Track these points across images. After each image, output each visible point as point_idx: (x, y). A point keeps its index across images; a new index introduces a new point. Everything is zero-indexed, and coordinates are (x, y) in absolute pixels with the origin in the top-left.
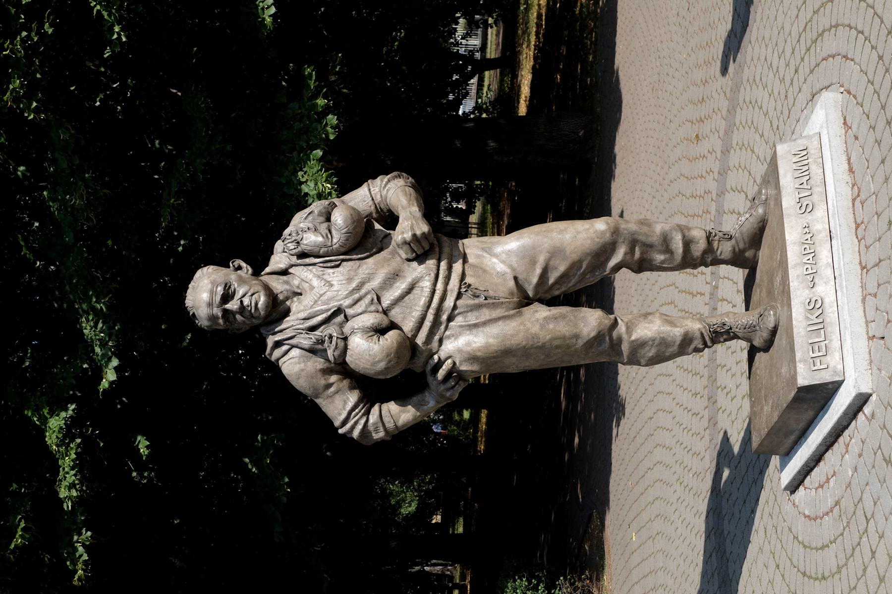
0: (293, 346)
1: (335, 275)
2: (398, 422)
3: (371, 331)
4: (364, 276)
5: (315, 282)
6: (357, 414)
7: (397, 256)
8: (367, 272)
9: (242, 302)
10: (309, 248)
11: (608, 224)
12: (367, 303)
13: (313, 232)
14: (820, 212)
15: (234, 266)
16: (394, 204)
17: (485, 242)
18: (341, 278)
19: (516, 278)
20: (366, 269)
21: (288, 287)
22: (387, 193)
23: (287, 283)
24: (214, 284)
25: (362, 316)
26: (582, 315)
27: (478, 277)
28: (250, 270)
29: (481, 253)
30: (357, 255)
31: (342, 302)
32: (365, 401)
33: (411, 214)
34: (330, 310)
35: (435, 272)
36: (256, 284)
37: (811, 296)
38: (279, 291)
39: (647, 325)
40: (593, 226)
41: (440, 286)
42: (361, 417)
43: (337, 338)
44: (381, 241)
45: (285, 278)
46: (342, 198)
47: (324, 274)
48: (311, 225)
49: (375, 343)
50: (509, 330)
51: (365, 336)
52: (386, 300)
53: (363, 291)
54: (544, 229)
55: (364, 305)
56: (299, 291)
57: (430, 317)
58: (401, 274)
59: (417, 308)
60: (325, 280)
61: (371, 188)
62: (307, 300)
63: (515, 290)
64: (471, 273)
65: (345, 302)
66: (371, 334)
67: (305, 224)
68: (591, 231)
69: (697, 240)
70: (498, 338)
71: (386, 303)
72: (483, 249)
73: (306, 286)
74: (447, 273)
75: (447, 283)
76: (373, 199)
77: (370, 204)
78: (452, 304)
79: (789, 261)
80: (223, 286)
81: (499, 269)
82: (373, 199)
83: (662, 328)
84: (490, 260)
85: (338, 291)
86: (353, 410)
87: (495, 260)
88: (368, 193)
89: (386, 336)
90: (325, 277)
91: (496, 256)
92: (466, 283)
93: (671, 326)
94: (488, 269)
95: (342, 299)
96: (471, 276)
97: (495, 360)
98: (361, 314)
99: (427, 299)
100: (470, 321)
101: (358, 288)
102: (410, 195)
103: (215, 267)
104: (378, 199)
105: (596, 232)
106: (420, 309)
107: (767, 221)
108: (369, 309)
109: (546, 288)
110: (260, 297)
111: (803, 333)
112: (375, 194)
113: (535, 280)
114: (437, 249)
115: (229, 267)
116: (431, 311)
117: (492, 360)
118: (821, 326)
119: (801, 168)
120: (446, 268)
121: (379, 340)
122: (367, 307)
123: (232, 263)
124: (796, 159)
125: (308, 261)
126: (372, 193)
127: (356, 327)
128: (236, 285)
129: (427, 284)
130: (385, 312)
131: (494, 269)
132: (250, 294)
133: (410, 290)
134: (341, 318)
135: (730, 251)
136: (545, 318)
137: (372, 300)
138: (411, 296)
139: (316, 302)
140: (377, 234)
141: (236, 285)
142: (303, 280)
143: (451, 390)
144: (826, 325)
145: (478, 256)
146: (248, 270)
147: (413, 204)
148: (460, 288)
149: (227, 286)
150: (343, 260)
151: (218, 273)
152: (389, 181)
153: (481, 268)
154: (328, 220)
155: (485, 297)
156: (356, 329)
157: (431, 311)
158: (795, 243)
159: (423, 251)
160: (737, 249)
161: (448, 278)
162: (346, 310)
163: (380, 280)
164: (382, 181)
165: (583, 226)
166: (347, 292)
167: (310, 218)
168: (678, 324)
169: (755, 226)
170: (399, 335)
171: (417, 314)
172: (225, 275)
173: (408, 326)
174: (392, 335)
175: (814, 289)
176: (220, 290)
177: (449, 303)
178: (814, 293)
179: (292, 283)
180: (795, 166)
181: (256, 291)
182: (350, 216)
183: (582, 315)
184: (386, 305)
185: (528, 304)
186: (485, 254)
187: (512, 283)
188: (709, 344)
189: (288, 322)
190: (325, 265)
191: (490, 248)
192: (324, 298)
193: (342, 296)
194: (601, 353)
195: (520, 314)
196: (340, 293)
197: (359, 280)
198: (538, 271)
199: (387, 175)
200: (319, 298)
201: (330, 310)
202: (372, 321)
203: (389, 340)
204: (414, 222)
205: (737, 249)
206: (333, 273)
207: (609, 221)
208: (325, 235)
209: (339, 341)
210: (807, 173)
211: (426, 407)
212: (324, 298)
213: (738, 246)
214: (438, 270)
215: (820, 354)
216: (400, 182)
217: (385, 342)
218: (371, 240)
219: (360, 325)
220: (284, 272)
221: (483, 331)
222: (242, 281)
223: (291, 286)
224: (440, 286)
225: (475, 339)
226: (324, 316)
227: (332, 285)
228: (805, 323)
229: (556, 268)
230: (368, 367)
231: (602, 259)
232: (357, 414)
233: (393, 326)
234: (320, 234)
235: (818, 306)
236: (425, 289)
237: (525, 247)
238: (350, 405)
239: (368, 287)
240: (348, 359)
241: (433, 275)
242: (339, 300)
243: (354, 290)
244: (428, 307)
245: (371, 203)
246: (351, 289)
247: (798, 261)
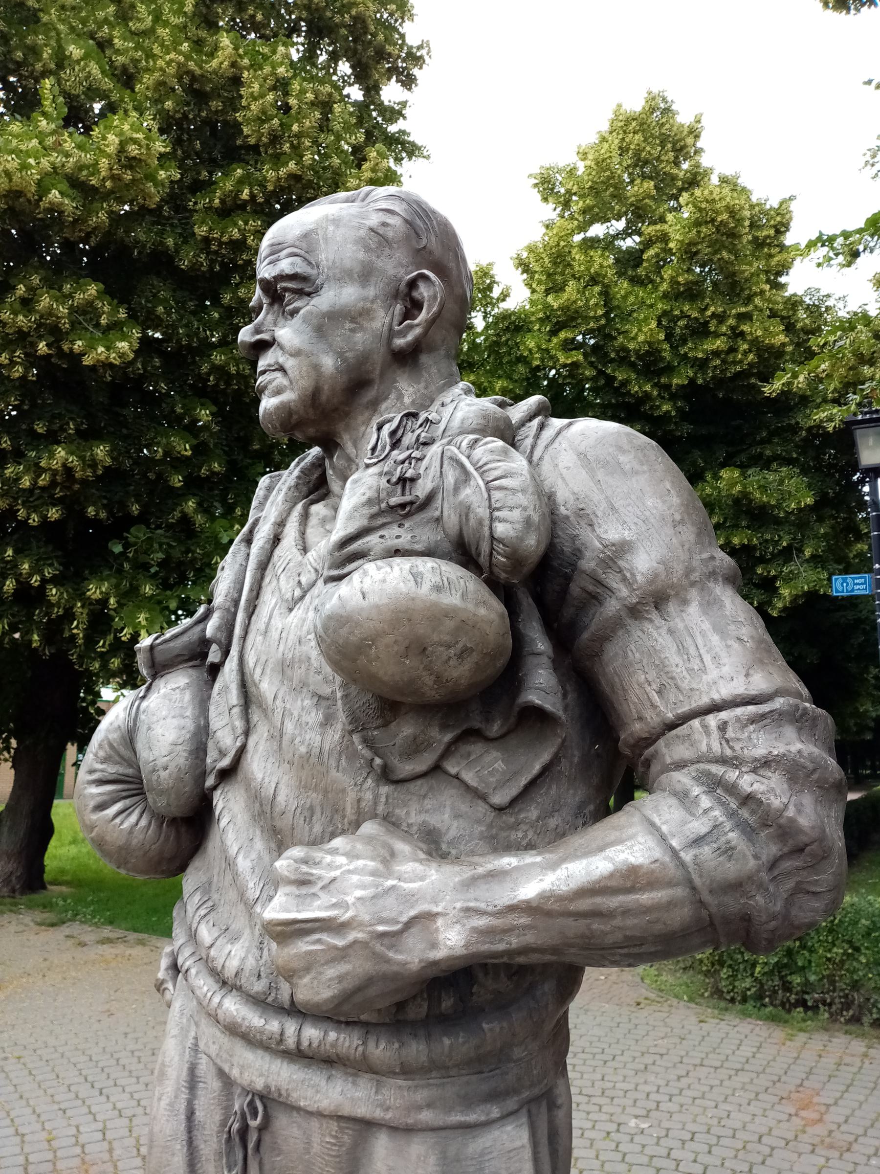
76: (672, 726)
77: (649, 714)
82: (672, 726)
88: (704, 700)
126: (696, 723)
245: (653, 719)
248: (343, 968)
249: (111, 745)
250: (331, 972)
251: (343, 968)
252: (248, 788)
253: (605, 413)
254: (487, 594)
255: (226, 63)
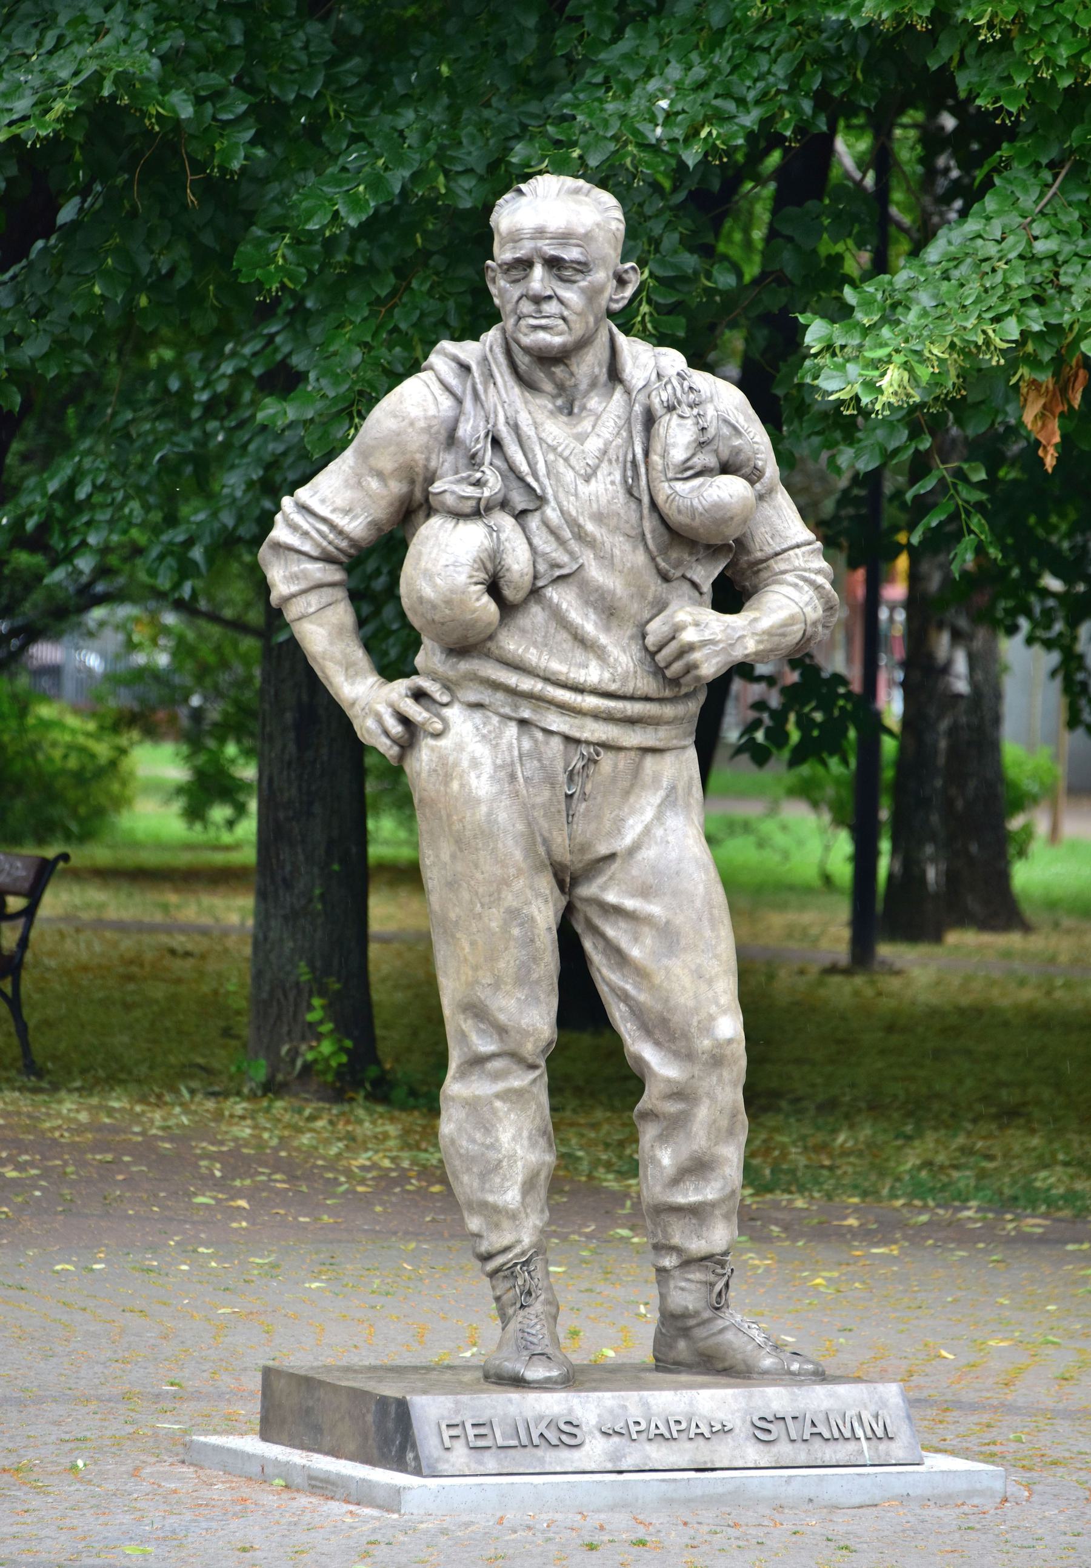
0: (459, 401)
1: (609, 486)
2: (311, 622)
3: (495, 567)
4: (608, 546)
5: (593, 445)
6: (324, 537)
7: (654, 611)
8: (617, 552)
9: (550, 298)
10: (662, 431)
11: (730, 1041)
12: (554, 555)
13: (695, 440)
14: (753, 1454)
15: (626, 271)
16: (764, 600)
17: (689, 793)
18: (603, 501)
19: (612, 856)
20: (622, 551)
21: (584, 386)
22: (791, 585)
23: (593, 385)
24: (586, 238)
25: (526, 546)
26: (542, 996)
27: (614, 780)
28: (616, 307)
29: (665, 784)
30: (653, 531)
31: (553, 503)
32: (352, 551)
33: (740, 638)
34: (537, 479)
35: (620, 693)
36: (587, 323)
37: (585, 1428)
38: (574, 368)
39: (525, 1134)
40: (725, 1012)
41: (591, 702)
42: (318, 545)
43: (480, 499)
44: (684, 576)
45: (604, 377)
46: (781, 488)
47: (610, 461)
48: (711, 432)
49: (471, 577)
50: (505, 846)
51: (484, 556)
52: (559, 594)
53: (574, 545)
54: (716, 912)
55: (548, 550)
56: (576, 410)
57: (527, 684)
58: (614, 623)
59: (545, 657)
60: (598, 467)
61: (804, 549)
62: (555, 430)
63: (590, 856)
64: (621, 765)
65: (554, 510)
66: (489, 566)
67: (715, 422)
68: (713, 1009)
69: (705, 1234)
70: (489, 822)
71: (553, 594)
72: (673, 789)
73: (586, 425)
74: (619, 716)
75: (596, 715)
76: (777, 554)
77: (766, 548)
78: (554, 728)
79: (656, 1393)
80: (582, 259)
81: (631, 822)
82: (777, 554)
83: (519, 1164)
84: (649, 804)
85: (576, 495)
86: (333, 527)
87: (649, 814)
88: (793, 542)
89: (486, 598)
90: (605, 465)
91: (659, 817)
92: (598, 754)
93: (524, 1184)
94: (632, 799)
95: (559, 504)
96: (615, 766)
97: (445, 818)
98: (530, 544)
99: (563, 678)
100: (522, 765)
101: (581, 535)
102: (784, 635)
103: (621, 234)
104: (778, 565)
105: (712, 1018)
106: (543, 663)
107: (749, 1378)
108: (540, 560)
109: (598, 922)
110: (561, 334)
111: (512, 1410)
112: (788, 559)
113: (611, 897)
114: (667, 693)
115: (623, 260)
116: (538, 686)
117: (443, 813)
118: (525, 1440)
119: (848, 1425)
120: (629, 713)
121: (476, 583)
122: (544, 554)
123: (633, 268)
124: (867, 1416)
125: (638, 427)
126: (791, 553)
127: (503, 536)
128: (583, 284)
129: (593, 674)
130: (535, 592)
131: (633, 812)
132: (566, 313)
133: (581, 640)
134: (520, 501)
135: (687, 1308)
136: (532, 919)
137: (559, 566)
138: (568, 645)
139: (554, 449)
140: (700, 568)
141: (583, 284)
142: (598, 417)
143: (379, 731)
144: (527, 1450)
145: (656, 779)
146: (617, 301)
147: (759, 642)
148: (588, 743)
149: (583, 267)
150: (639, 501)
151: (609, 242)
152: (818, 588)
153: (632, 786)
154: (726, 468)
155: (572, 795)
156: (498, 538)
157: (538, 686)
158: (691, 1404)
159: (662, 665)
160: (692, 1322)
161: (608, 718)
162: (537, 514)
163: (601, 579)
164: (819, 572)
165: (725, 992)
166: (574, 513)
167: (726, 431)
168: (529, 1200)
169: (739, 1356)
170: (490, 624)
171: (532, 656)
172: (604, 259)
173: (511, 644)
174: (487, 606)
175: (598, 1434)
176: (572, 254)
177: (556, 722)
178: (591, 1433)
179: (592, 394)
180: (851, 1413)
181: (572, 325)
182: (729, 514)
183: (542, 996)
184: (548, 594)
185: (561, 884)
186: (662, 793)
187: (603, 850)
188: (491, 1265)
189: (514, 393)
190: (629, 465)
191: (674, 804)
192: (561, 466)
193: (565, 503)
194: (463, 1036)
195: (538, 868)
196: (572, 498)
197: (598, 536)
198: (630, 904)
199: (833, 584)
200: (561, 456)
201: (537, 479)
202: (515, 567)
203: (478, 604)
204: (721, 645)
205: (692, 1322)
206: (613, 483)
207: (735, 1045)
208: (690, 464)
209: (473, 503)
210: (836, 1435)
211: (342, 679)
212: (561, 466)
213: (698, 1325)
214: (631, 698)
215: (471, 1438)
216: (814, 612)
217: (474, 597)
218: (686, 557)
219: (507, 544)
220: (615, 374)
221: (501, 792)
222: (592, 294)
223: (586, 394)
224: (591, 702)
225: (485, 777)
226: (524, 468)
227: (587, 479)
228: (529, 1415)
229: (636, 939)
230: (423, 564)
231: (658, 1034)
232: (324, 537)
233: (507, 608)
234: (693, 455)
235: (564, 1438)
236: (583, 672)
237: (913, 1004)
238: (341, 521)
239: (588, 558)
240: (435, 522)
241: (613, 687)
242: (556, 498)
243: (579, 526)
244: (547, 680)
245: (769, 551)
246: (581, 520)
247: (655, 1409)
248: (718, 659)
249: (481, 560)
250: (714, 661)
251: (718, 659)
252: (645, 1369)
253: (608, 904)
254: (550, 948)
255: (995, 1258)
